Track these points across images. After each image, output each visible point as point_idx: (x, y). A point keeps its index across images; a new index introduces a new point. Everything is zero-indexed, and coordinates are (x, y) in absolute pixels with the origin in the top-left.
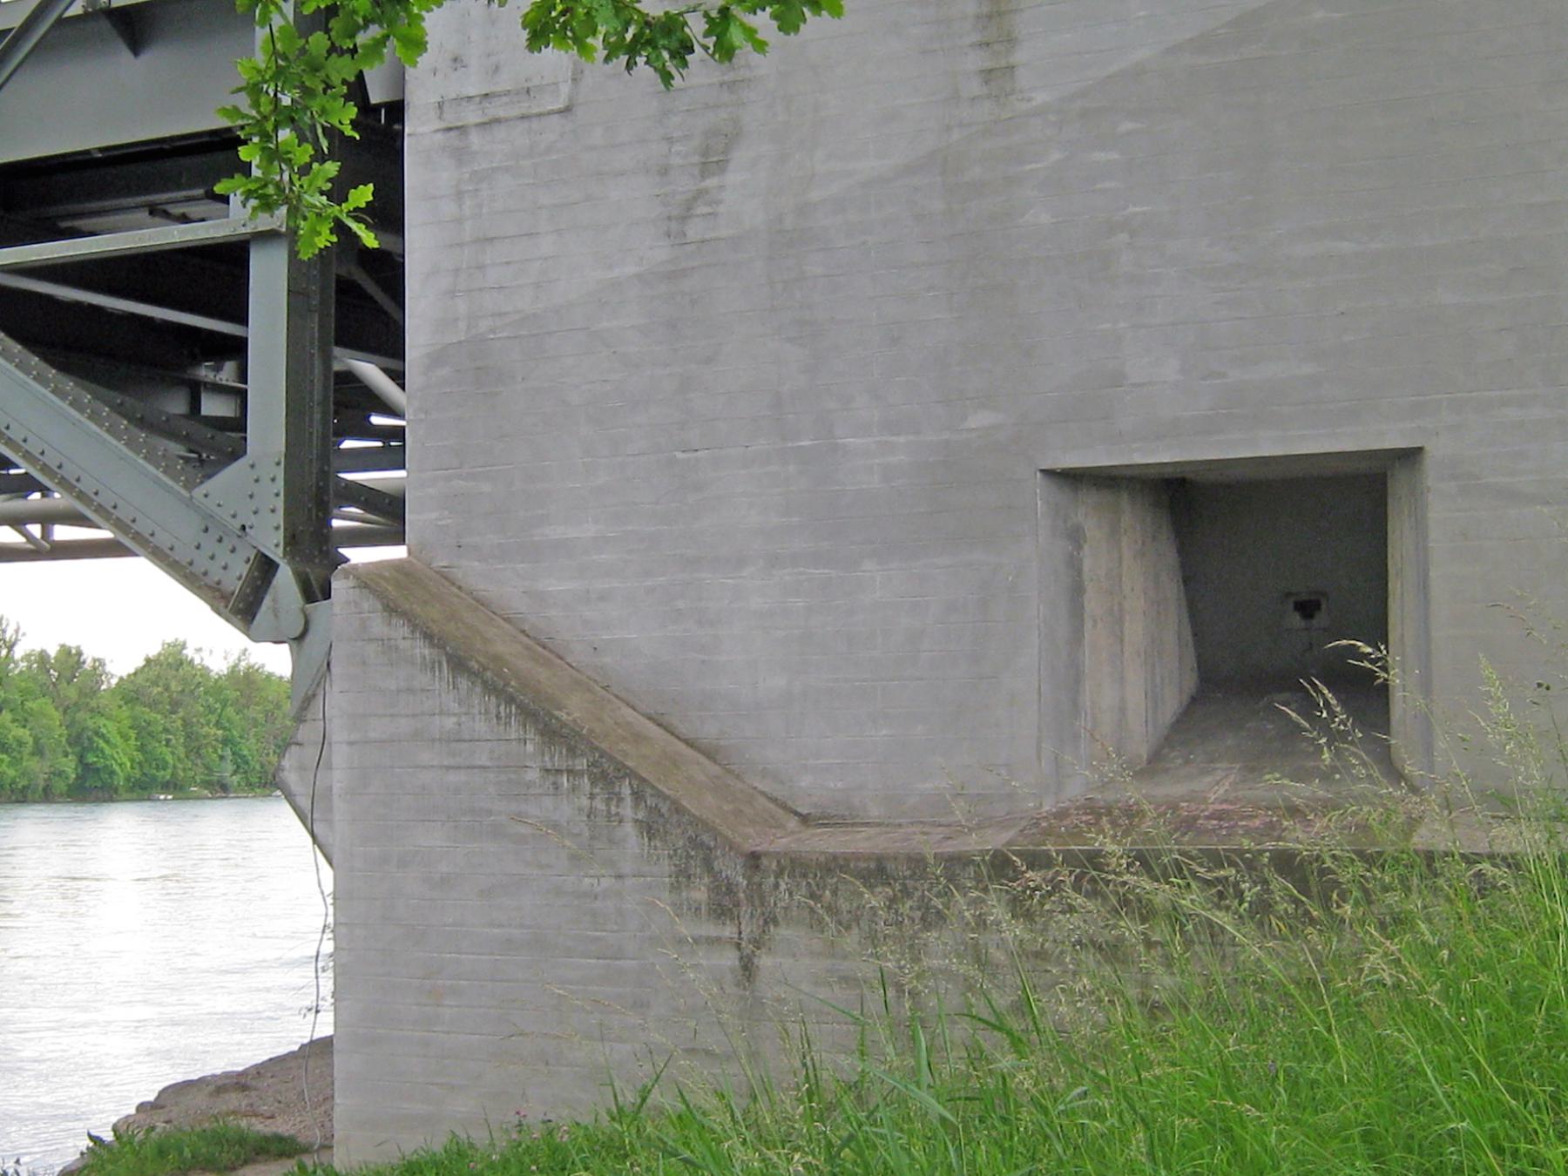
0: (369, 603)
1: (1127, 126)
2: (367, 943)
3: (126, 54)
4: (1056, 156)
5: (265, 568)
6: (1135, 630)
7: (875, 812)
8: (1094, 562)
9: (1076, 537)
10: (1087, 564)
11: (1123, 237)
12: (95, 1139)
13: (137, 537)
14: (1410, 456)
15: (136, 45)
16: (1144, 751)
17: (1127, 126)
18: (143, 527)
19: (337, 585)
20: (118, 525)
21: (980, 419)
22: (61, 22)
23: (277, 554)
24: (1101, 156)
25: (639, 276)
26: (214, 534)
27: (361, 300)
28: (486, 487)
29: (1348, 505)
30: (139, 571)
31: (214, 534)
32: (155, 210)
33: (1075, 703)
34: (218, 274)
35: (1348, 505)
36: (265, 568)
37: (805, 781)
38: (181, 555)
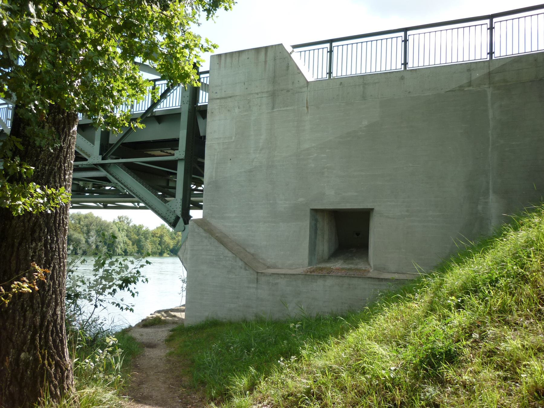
0: (195, 226)
1: (327, 150)
2: (193, 286)
3: (157, 124)
4: (316, 155)
5: (177, 218)
6: (326, 237)
7: (280, 266)
8: (319, 226)
9: (316, 220)
10: (318, 225)
11: (326, 170)
12: (332, 311)
13: (149, 206)
14: (372, 209)
15: (159, 123)
16: (327, 258)
17: (327, 150)
18: (150, 204)
19: (190, 222)
20: (145, 203)
21: (301, 200)
22: (147, 117)
23: (180, 216)
24: (323, 155)
25: (245, 172)
26: (169, 212)
27: (195, 170)
28: (217, 206)
29: (364, 216)
30: (149, 212)
31: (169, 212)
32: (161, 151)
33: (315, 249)
34: (173, 164)
35: (364, 216)
36: (177, 218)
37: (269, 260)
38: (164, 215)
